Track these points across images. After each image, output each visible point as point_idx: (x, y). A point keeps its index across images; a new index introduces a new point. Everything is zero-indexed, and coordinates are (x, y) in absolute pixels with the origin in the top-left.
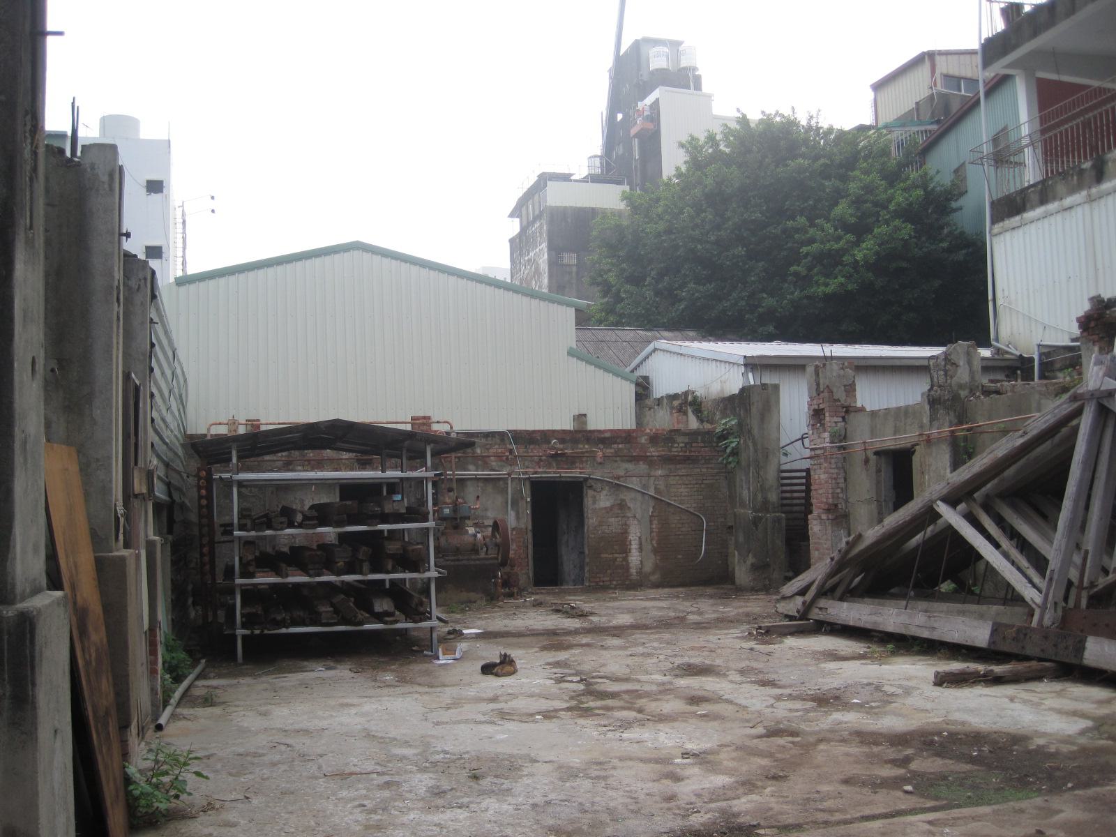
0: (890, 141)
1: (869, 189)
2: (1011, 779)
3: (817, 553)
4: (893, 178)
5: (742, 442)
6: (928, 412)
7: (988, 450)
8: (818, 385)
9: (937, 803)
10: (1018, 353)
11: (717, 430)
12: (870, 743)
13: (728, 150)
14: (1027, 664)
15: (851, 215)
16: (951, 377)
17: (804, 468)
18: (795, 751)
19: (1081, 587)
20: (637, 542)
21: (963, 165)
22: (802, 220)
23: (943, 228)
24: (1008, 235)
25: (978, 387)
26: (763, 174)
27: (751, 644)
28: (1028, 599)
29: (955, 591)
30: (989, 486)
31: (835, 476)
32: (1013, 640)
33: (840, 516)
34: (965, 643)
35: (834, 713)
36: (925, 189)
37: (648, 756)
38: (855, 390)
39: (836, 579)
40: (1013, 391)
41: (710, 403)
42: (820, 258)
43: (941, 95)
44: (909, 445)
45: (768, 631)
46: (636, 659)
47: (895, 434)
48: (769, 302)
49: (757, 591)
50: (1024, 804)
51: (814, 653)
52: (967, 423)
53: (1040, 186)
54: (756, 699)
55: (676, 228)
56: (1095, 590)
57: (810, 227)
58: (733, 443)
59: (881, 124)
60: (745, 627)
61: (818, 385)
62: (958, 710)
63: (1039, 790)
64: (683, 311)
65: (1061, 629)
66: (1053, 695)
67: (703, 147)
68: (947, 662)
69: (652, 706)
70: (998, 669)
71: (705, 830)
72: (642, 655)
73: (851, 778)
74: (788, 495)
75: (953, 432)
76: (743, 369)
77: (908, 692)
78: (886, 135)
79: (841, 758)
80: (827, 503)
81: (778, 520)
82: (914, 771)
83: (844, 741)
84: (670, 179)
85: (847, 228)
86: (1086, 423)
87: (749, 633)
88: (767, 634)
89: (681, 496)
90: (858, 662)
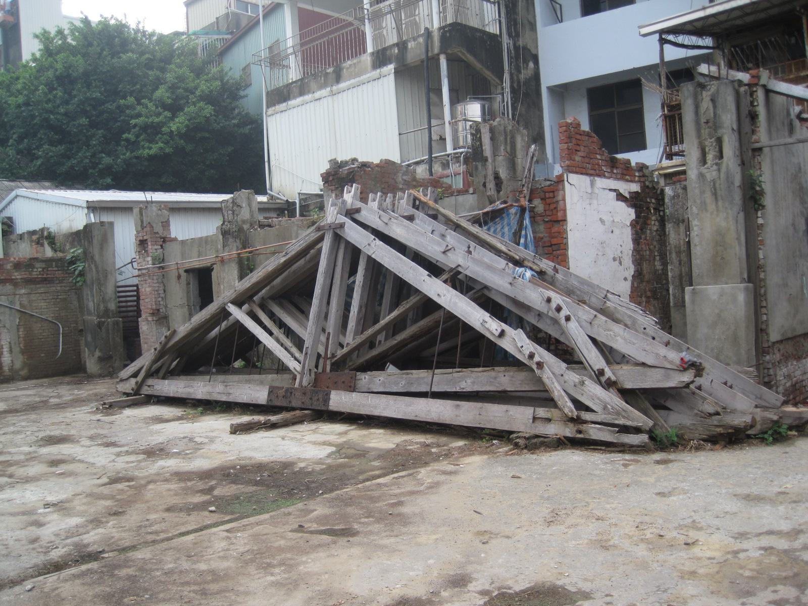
0: (197, 45)
1: (181, 79)
2: (282, 493)
3: (146, 345)
4: (199, 72)
5: (87, 265)
6: (222, 240)
7: (262, 267)
8: (142, 222)
9: (232, 517)
10: (285, 199)
11: (67, 258)
12: (185, 480)
13: (74, 43)
14: (293, 413)
15: (168, 98)
16: (237, 215)
17: (135, 284)
18: (131, 492)
19: (326, 358)
20: (8, 346)
21: (248, 65)
22: (131, 100)
23: (234, 109)
24: (278, 115)
25: (256, 222)
26: (102, 63)
27: (99, 416)
28: (292, 368)
29: (245, 366)
30: (264, 291)
31: (157, 289)
32: (283, 397)
33: (161, 318)
34: (251, 402)
35: (159, 461)
36: (222, 81)
37: (17, 510)
38: (169, 225)
39: (159, 364)
40: (279, 224)
41: (61, 237)
42: (145, 128)
43: (235, 15)
44: (209, 265)
45: (111, 406)
46: (8, 436)
47: (199, 257)
48: (107, 160)
49: (104, 377)
50: (291, 509)
51: (145, 418)
52: (249, 248)
53: (299, 83)
54: (101, 457)
55: (33, 102)
56: (336, 359)
57: (138, 104)
58: (80, 266)
59: (191, 31)
60: (94, 404)
61: (142, 222)
62: (247, 449)
63: (301, 498)
64: (40, 166)
65: (315, 387)
66: (310, 432)
67: (53, 39)
68: (240, 417)
69: (20, 472)
70: (273, 418)
71: (62, 560)
72: (13, 433)
73: (171, 507)
74: (124, 304)
75: (239, 254)
76: (86, 211)
77: (212, 440)
78: (194, 40)
79: (164, 493)
80: (152, 309)
81: (117, 323)
82: (217, 496)
83: (166, 480)
84: (28, 62)
85: (165, 107)
86: (326, 246)
87: (97, 409)
88: (110, 408)
89: (41, 308)
90: (177, 423)
